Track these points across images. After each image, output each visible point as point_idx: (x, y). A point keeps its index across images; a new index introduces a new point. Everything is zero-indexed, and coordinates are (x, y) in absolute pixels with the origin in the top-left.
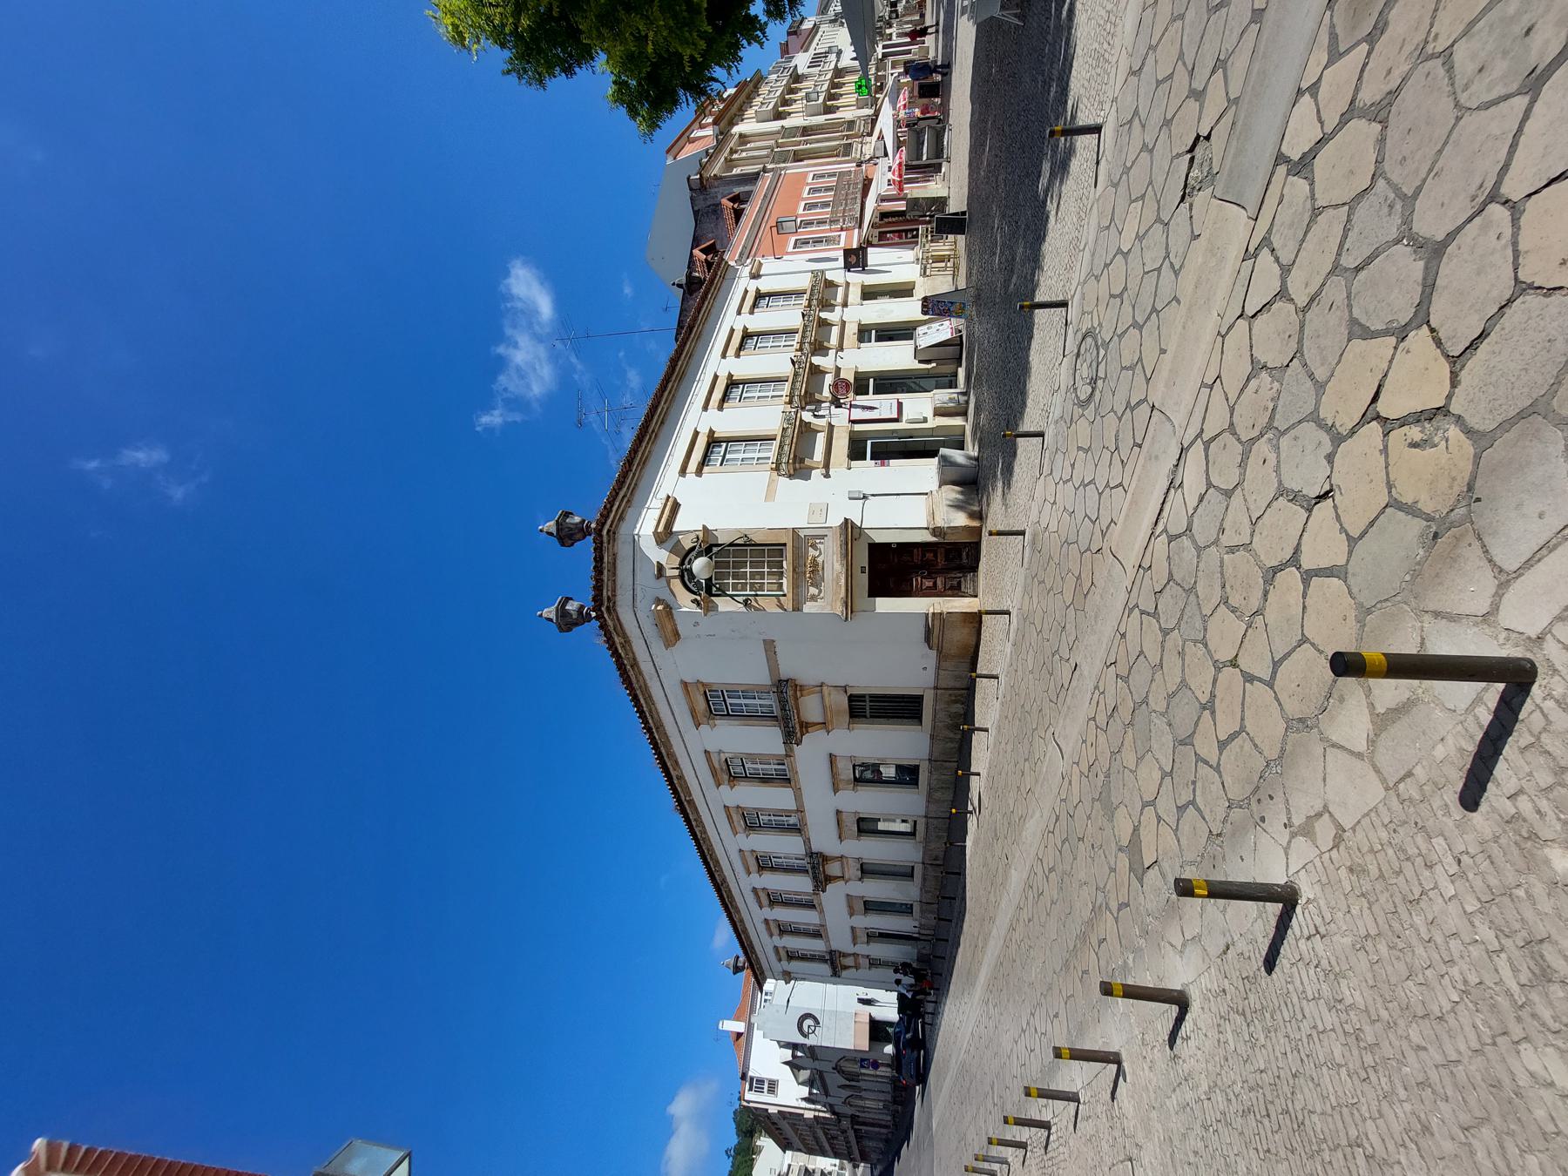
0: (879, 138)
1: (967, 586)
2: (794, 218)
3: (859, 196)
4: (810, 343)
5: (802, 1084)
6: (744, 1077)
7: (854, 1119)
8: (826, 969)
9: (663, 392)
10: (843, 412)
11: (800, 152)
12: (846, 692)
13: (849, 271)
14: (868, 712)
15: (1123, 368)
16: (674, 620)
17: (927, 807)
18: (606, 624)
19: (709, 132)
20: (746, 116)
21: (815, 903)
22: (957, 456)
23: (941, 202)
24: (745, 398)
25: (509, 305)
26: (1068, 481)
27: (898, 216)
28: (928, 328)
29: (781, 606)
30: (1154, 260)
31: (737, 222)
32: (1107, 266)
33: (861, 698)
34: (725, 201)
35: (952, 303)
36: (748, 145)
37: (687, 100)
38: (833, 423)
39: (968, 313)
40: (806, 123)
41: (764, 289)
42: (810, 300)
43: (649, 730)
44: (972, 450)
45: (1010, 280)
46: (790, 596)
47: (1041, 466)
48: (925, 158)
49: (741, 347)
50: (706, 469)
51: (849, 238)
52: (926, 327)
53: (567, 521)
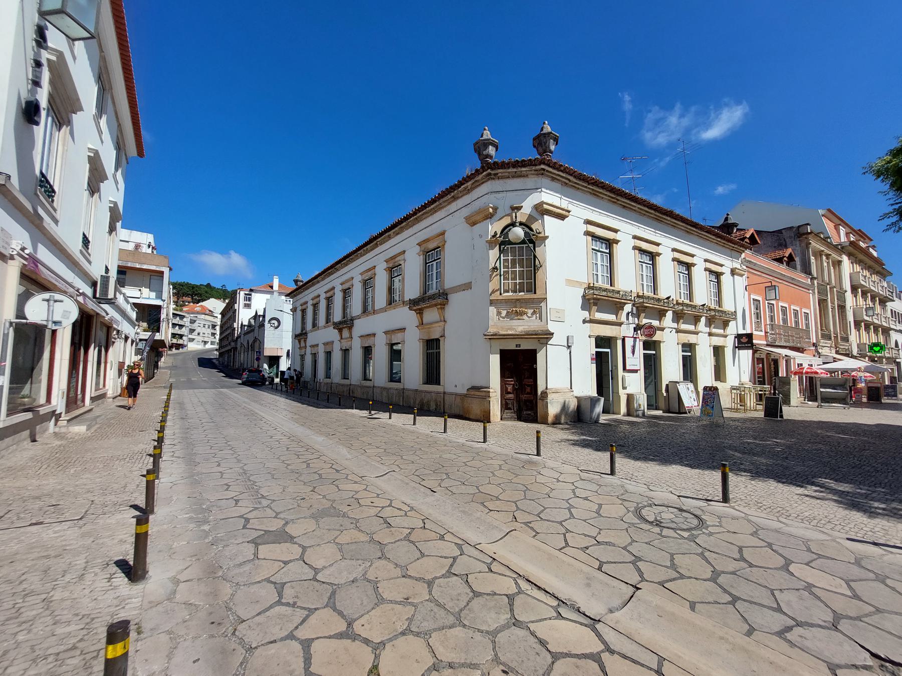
0: (835, 358)
1: (508, 413)
2: (778, 298)
3: (791, 344)
4: (683, 310)
5: (249, 322)
6: (251, 290)
7: (235, 349)
8: (299, 331)
9: (647, 207)
10: (631, 332)
11: (825, 304)
12: (441, 337)
13: (735, 337)
14: (432, 351)
15: (672, 555)
16: (483, 221)
17: (379, 387)
18: (479, 174)
19: (843, 239)
20: (855, 265)
21: (329, 324)
22: (599, 408)
23: (787, 401)
24: (642, 265)
25: (711, 107)
26: (574, 494)
27: (775, 372)
28: (692, 391)
29: (493, 292)
30: (788, 603)
31: (774, 260)
32: (770, 545)
33: (438, 347)
34: (789, 251)
35: (713, 407)
36: (832, 268)
37: (897, 204)
38: (619, 232)
39: (704, 418)
40: (848, 307)
41: (723, 278)
42: (715, 310)
43: (415, 213)
44: (604, 419)
45: (736, 451)
46: (500, 298)
47: (587, 471)
48: (822, 390)
49: (680, 263)
50: (590, 238)
51: (760, 338)
52: (693, 389)
53: (551, 140)
